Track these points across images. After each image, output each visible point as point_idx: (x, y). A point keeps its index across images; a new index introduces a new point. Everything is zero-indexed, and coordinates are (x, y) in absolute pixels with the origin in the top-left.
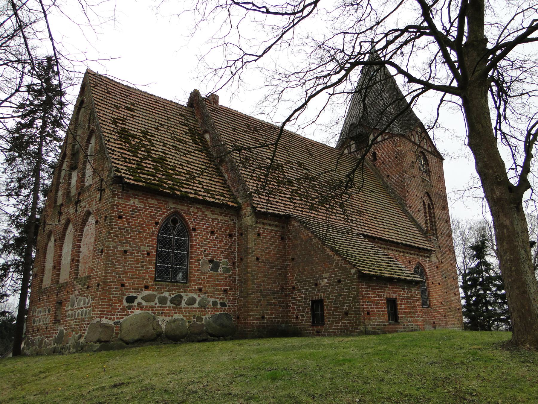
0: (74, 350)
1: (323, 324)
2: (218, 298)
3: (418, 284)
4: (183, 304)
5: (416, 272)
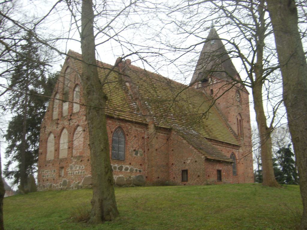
0: (76, 189)
1: (187, 181)
2: (138, 168)
3: (232, 163)
4: (123, 170)
5: (231, 157)
